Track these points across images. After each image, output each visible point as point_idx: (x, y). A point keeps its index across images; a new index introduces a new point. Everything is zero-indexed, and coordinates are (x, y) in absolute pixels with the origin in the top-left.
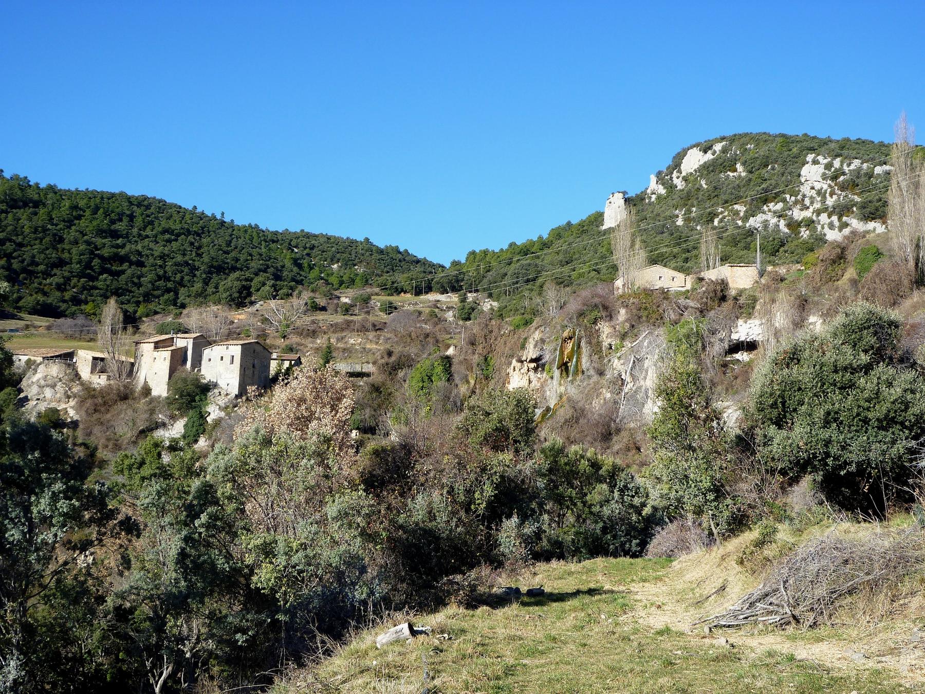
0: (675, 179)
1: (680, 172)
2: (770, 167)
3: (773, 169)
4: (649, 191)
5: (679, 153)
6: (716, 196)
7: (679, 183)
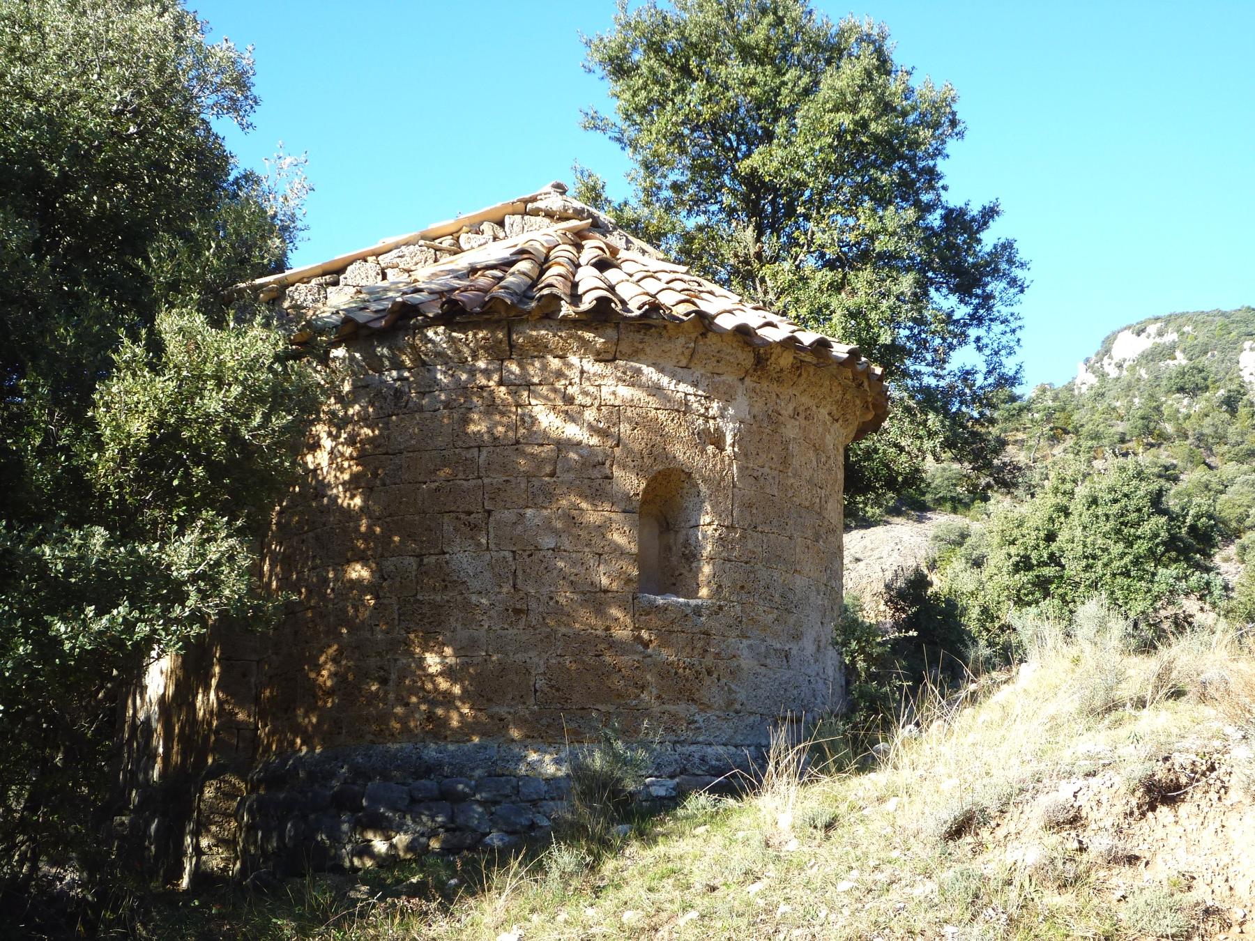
0: (1106, 366)
1: (1111, 358)
2: (1209, 354)
3: (1213, 356)
4: (1078, 382)
5: (1108, 337)
6: (1158, 385)
7: (1113, 372)
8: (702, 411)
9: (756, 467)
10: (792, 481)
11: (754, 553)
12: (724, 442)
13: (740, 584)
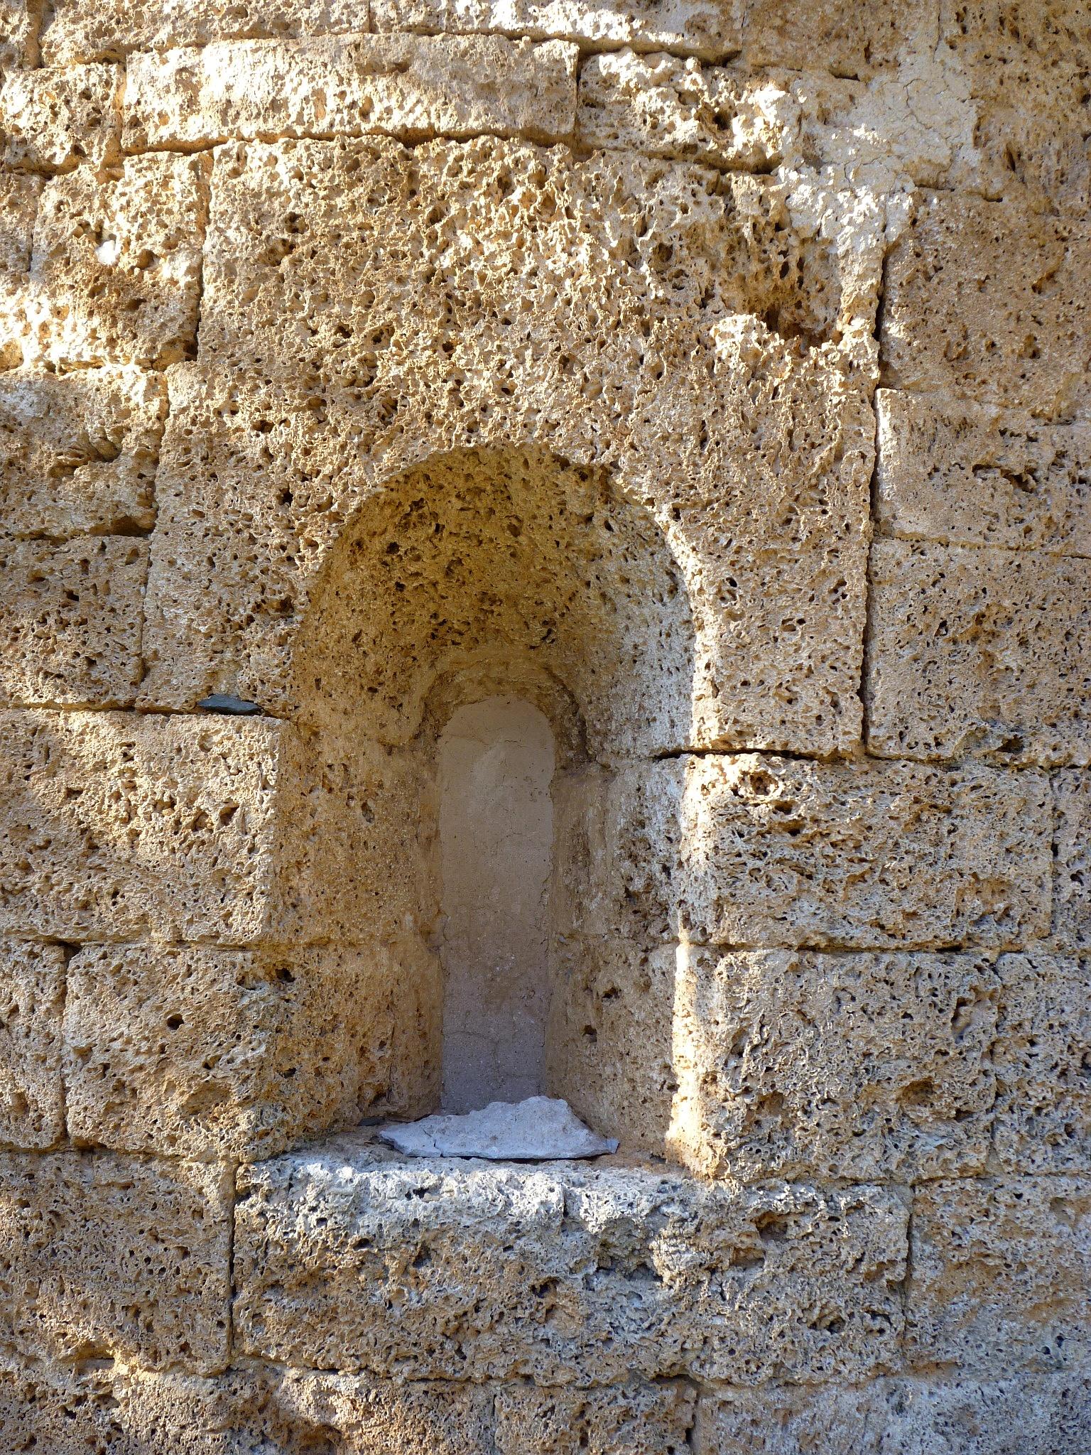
8: (686, 129)
9: (1021, 422)
10: (406, 248)
11: (1002, 887)
12: (827, 289)
13: (901, 1072)
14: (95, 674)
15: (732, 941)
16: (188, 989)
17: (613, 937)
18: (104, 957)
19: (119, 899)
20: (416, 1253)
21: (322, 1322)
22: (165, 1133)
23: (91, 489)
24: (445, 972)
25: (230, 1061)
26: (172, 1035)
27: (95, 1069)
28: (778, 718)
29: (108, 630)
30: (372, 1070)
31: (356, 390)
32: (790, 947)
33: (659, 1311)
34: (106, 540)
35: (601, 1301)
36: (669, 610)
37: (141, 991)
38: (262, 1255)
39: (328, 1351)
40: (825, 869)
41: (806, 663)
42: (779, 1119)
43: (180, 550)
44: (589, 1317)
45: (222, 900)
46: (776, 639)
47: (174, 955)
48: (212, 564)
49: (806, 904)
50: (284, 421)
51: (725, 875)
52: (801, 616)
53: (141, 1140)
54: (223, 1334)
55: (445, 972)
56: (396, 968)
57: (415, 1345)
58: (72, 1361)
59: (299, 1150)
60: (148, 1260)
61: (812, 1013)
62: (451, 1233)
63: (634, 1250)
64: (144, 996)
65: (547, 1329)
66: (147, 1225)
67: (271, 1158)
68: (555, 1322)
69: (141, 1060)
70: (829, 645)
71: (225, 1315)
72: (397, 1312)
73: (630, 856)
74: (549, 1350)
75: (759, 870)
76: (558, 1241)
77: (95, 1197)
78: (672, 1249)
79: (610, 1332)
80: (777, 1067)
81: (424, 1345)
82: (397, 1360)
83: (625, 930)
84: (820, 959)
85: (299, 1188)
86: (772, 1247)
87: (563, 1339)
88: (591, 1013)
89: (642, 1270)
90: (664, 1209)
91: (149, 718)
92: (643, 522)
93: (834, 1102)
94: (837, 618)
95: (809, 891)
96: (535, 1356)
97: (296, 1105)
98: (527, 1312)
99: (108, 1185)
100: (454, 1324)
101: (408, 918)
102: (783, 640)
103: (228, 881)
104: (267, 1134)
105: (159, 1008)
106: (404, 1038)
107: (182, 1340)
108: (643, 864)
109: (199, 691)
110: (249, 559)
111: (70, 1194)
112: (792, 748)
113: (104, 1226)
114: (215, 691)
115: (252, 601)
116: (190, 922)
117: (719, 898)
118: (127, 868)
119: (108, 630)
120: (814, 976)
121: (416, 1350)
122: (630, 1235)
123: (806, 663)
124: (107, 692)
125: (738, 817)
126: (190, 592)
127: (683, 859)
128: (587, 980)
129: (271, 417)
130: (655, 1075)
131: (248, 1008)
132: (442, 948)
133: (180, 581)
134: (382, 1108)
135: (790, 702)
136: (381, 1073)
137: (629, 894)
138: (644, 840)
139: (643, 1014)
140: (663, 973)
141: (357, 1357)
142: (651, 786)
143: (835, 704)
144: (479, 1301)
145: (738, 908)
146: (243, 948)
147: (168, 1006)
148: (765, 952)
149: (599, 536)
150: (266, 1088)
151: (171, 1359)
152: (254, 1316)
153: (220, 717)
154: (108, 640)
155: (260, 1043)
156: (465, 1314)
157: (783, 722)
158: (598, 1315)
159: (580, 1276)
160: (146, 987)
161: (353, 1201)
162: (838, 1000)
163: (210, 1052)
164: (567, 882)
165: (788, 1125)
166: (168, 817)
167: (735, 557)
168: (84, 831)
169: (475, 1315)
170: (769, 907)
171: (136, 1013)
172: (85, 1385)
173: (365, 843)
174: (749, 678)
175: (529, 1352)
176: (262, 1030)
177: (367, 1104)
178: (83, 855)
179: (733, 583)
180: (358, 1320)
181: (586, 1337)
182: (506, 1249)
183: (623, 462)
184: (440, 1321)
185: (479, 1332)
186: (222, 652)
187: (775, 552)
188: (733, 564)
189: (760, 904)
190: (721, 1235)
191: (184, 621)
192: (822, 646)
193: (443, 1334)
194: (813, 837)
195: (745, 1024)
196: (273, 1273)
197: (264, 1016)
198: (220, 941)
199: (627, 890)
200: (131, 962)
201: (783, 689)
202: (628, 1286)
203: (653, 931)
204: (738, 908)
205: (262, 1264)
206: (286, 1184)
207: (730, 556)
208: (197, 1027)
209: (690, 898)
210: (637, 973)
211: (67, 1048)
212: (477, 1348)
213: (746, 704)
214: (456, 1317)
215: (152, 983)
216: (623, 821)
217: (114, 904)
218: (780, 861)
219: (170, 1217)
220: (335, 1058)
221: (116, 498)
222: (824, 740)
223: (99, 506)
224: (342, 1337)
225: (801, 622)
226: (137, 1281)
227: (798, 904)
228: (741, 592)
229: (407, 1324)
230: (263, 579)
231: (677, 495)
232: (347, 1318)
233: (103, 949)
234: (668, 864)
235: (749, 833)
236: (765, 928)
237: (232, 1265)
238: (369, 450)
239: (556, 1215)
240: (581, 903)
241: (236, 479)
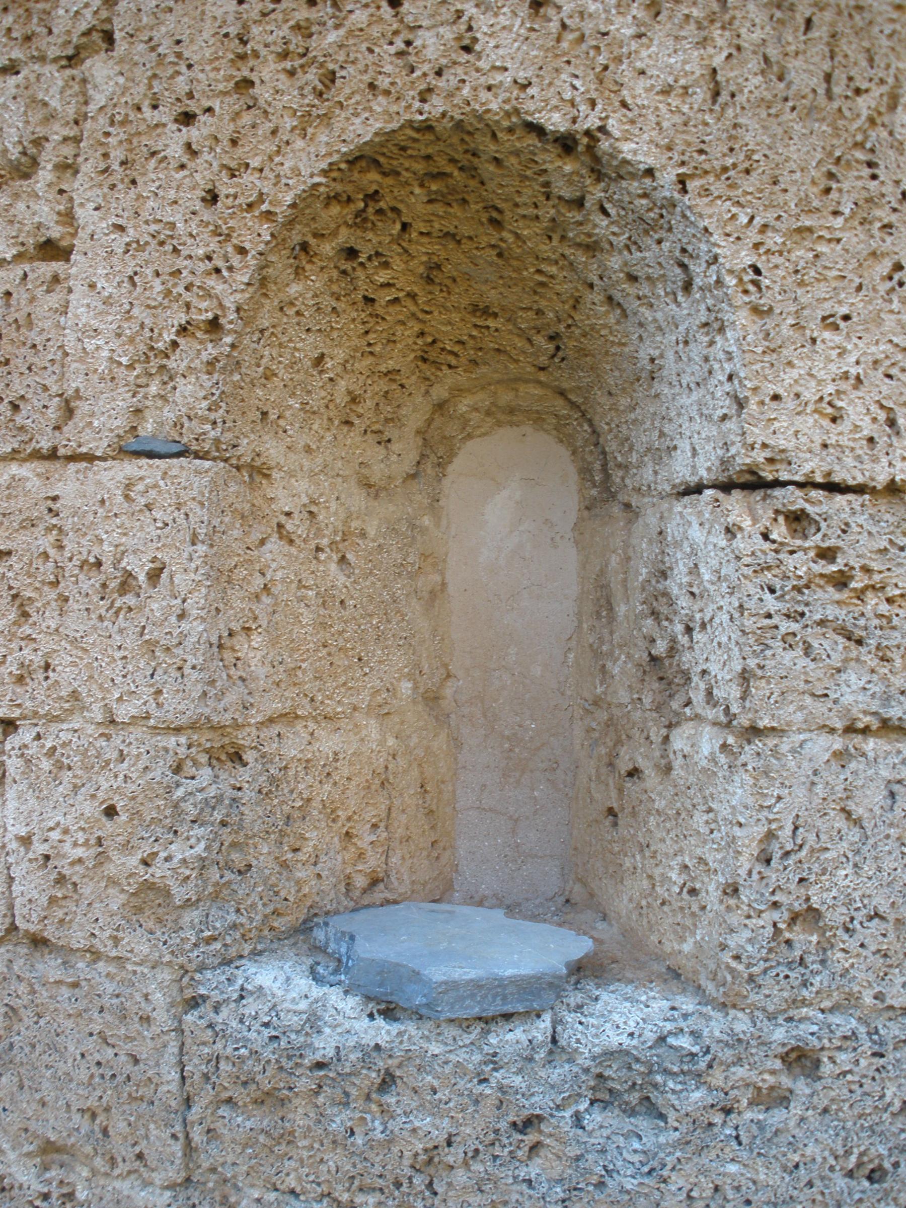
14: (19, 420)
15: (761, 724)
16: (121, 777)
17: (635, 709)
18: (38, 737)
19: (51, 674)
20: (379, 1081)
21: (279, 1143)
22: (107, 933)
23: (13, 211)
24: (457, 743)
25: (168, 859)
26: (109, 826)
27: (36, 859)
28: (818, 441)
29: (30, 369)
30: (361, 855)
31: (288, 65)
32: (832, 731)
33: (662, 1155)
34: (27, 267)
35: (593, 1141)
36: (685, 312)
37: (74, 777)
38: (212, 1070)
39: (288, 1174)
40: (878, 632)
41: (853, 371)
42: (814, 938)
43: (99, 271)
44: (578, 1158)
45: (152, 675)
46: (814, 341)
47: (108, 737)
48: (134, 285)
49: (853, 678)
50: (209, 110)
51: (751, 641)
52: (844, 310)
53: (84, 938)
54: (177, 1148)
55: (457, 743)
56: (391, 742)
57: (381, 1176)
58: (37, 1156)
59: (260, 953)
60: (99, 1064)
61: (859, 811)
62: (418, 1061)
63: (634, 1084)
64: (78, 782)
65: (531, 1169)
66: (96, 1028)
67: (221, 964)
68: (539, 1161)
69: (80, 852)
70: (882, 347)
71: (178, 1128)
72: (359, 1140)
73: (653, 613)
74: (532, 1192)
75: (794, 635)
76: (543, 1074)
77: (45, 994)
78: (679, 1087)
79: (602, 1176)
80: (813, 878)
81: (391, 1178)
82: (361, 1190)
83: (647, 700)
84: (871, 745)
85: (251, 1000)
86: (802, 1087)
87: (548, 1181)
88: (614, 794)
89: (646, 1103)
90: (671, 1040)
91: (72, 467)
92: (644, 202)
93: (882, 918)
94: (892, 312)
95: (858, 660)
96: (515, 1197)
97: (253, 906)
98: (506, 1150)
99: (56, 982)
100: (423, 1157)
101: (406, 687)
102: (823, 341)
103: (158, 654)
104: (216, 939)
105: (93, 796)
106: (403, 818)
107: (137, 1149)
108: (666, 623)
109: (121, 432)
110: (172, 274)
111: (22, 988)
112: (836, 478)
113: (56, 1025)
114: (141, 432)
115: (176, 323)
116: (120, 699)
117: (744, 670)
118: (56, 638)
119: (30, 369)
120: (861, 767)
121: (381, 1182)
122: (630, 1068)
123: (853, 371)
124: (31, 440)
125: (769, 568)
126: (110, 318)
127: (707, 619)
128: (609, 755)
129: (192, 106)
130: (674, 876)
131: (183, 799)
132: (453, 716)
133: (101, 307)
134: (380, 893)
135: (834, 420)
136: (373, 861)
137: (653, 659)
138: (666, 594)
139: (663, 802)
140: (685, 756)
141: (319, 1184)
142: (673, 530)
143: (892, 423)
144: (450, 1135)
145: (769, 683)
146: (178, 730)
147: (101, 795)
148: (802, 737)
149: (595, 226)
150: (210, 889)
151: (126, 1167)
152: (209, 1131)
153: (144, 461)
154: (29, 381)
155: (199, 840)
156: (436, 1147)
157: (825, 446)
158: (589, 1157)
159: (568, 1114)
160: (79, 772)
161: (308, 1020)
162: (892, 795)
163: (146, 849)
164: (591, 641)
165: (826, 945)
166: (96, 580)
167: (758, 238)
168: (15, 597)
169: (446, 1150)
170: (807, 682)
171: (71, 802)
172: (49, 1182)
173: (342, 602)
174: (781, 391)
175: (509, 1192)
176: (201, 825)
177: (357, 893)
178: (15, 623)
179: (757, 272)
180: (316, 1146)
181: (574, 1181)
182: (481, 1082)
183: (613, 125)
184: (407, 1154)
185: (452, 1167)
186: (148, 385)
187: (810, 230)
188: (757, 246)
189: (796, 678)
190: (740, 1072)
191: (105, 354)
192: (873, 349)
193: (413, 1167)
194: (863, 590)
195: (774, 826)
196: (225, 1088)
197: (202, 810)
198: (152, 722)
199: (650, 654)
200: (64, 745)
201: (824, 405)
202: (629, 1123)
203: (675, 705)
204: (769, 683)
205: (214, 1078)
206: (235, 996)
207: (753, 236)
208: (132, 820)
209: (714, 668)
210: (658, 754)
211: (9, 836)
212: (450, 1184)
213: (777, 424)
214: (426, 1150)
215: (88, 768)
216: (644, 571)
217: (47, 678)
218: (822, 623)
219: (117, 1023)
220: (308, 848)
221: (37, 219)
222: (878, 468)
223: (20, 230)
224: (301, 1160)
225: (846, 318)
226: (90, 1084)
227: (844, 676)
228: (767, 282)
229: (370, 1155)
230: (187, 296)
231: (683, 163)
232: (305, 1143)
233: (38, 729)
234: (691, 625)
235: (782, 588)
236: (801, 708)
237: (183, 1078)
238: (305, 135)
239: (540, 1046)
240: (604, 666)
241: (157, 184)
